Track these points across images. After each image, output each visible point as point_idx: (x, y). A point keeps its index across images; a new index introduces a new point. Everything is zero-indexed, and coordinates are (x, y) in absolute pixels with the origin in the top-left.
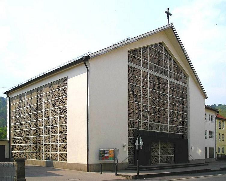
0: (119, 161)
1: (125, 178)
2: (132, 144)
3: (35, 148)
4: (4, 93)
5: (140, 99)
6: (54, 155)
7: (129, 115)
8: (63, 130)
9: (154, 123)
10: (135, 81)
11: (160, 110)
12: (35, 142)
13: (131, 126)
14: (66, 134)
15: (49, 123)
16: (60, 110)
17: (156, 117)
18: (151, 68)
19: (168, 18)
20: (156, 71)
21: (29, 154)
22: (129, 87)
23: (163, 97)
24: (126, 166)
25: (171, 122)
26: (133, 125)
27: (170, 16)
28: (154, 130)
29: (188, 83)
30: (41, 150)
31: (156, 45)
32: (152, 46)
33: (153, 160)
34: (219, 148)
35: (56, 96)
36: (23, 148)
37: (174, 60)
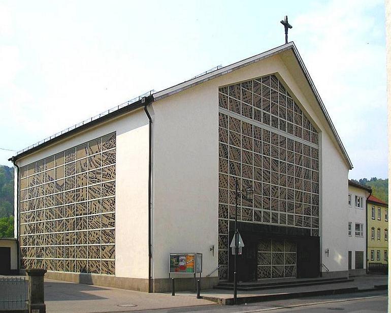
0: (204, 275)
1: (213, 303)
2: (226, 246)
3: (61, 252)
4: (9, 160)
5: (239, 169)
6: (92, 264)
7: (220, 196)
8: (108, 221)
9: (262, 210)
10: (231, 140)
11: (272, 188)
12: (62, 242)
13: (224, 215)
14: (114, 228)
15: (84, 210)
16: (104, 188)
17: (266, 199)
18: (257, 117)
19: (286, 33)
20: (266, 121)
21: (52, 262)
22: (220, 148)
23: (277, 166)
24: (216, 282)
25: (291, 208)
26: (227, 213)
27: (289, 29)
28: (262, 222)
29: (319, 143)
30: (71, 255)
31: (266, 78)
32: (259, 79)
33: (260, 273)
34: (372, 253)
35: (96, 164)
36: (41, 251)
37: (295, 104)
